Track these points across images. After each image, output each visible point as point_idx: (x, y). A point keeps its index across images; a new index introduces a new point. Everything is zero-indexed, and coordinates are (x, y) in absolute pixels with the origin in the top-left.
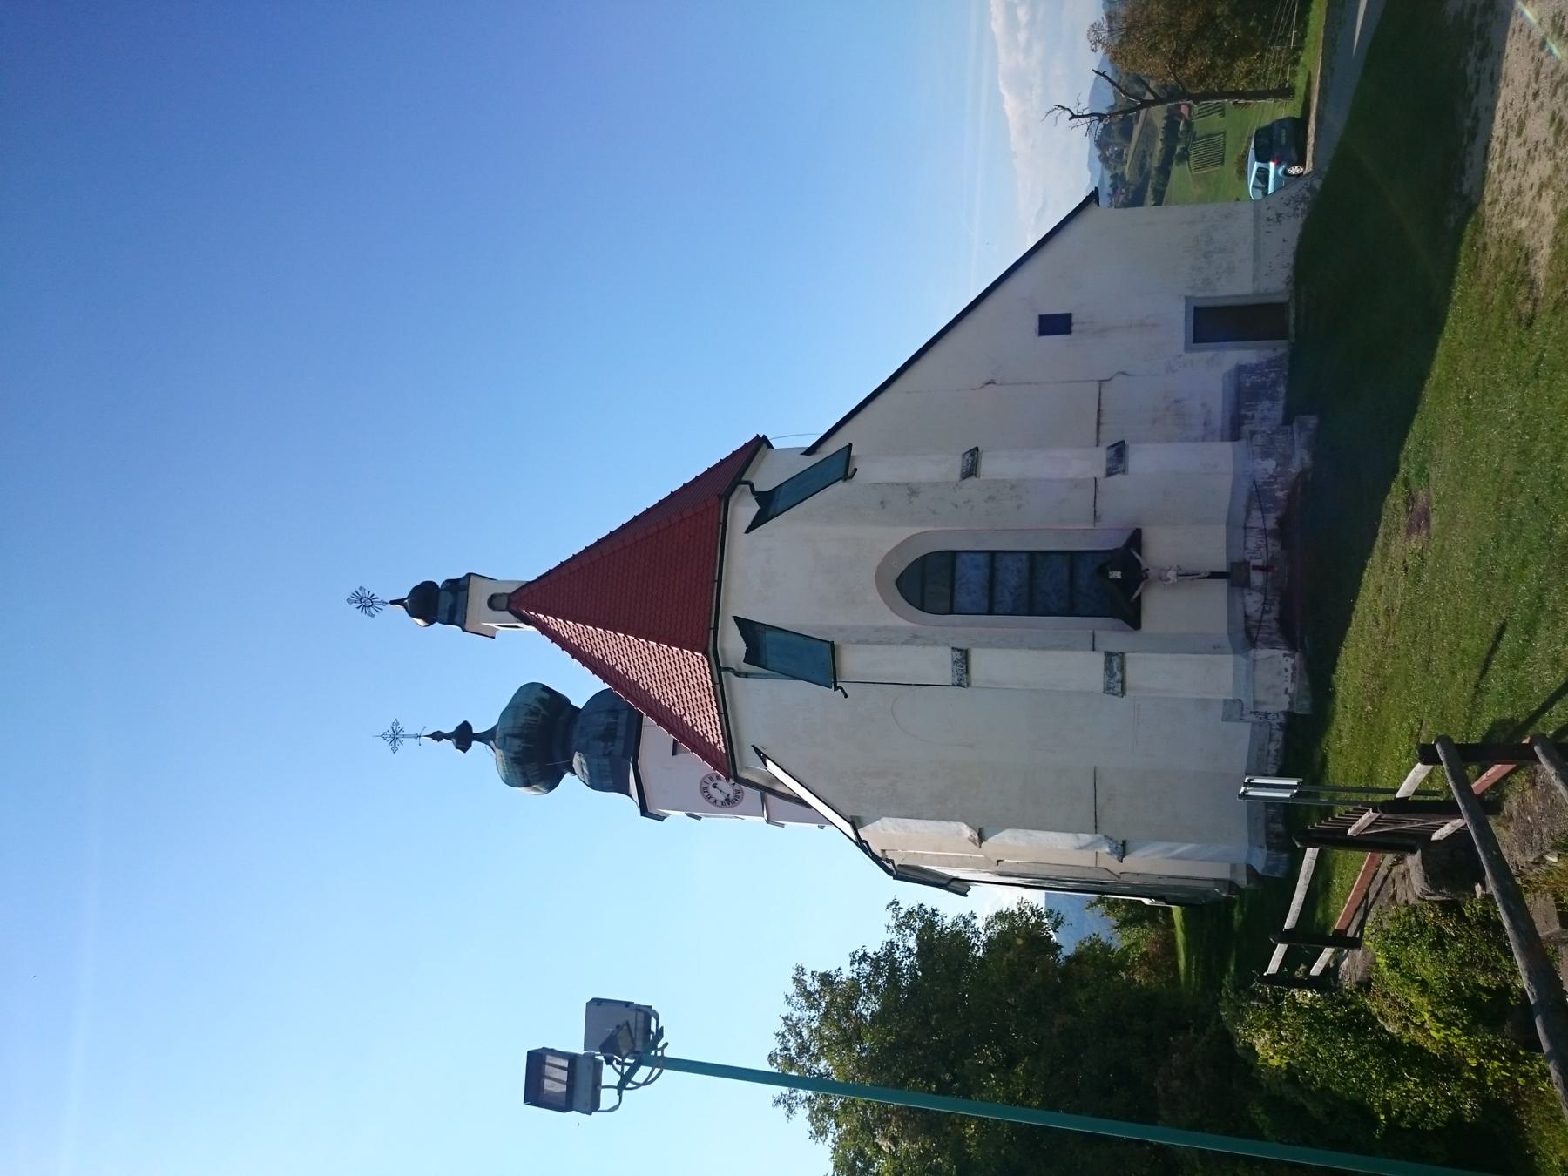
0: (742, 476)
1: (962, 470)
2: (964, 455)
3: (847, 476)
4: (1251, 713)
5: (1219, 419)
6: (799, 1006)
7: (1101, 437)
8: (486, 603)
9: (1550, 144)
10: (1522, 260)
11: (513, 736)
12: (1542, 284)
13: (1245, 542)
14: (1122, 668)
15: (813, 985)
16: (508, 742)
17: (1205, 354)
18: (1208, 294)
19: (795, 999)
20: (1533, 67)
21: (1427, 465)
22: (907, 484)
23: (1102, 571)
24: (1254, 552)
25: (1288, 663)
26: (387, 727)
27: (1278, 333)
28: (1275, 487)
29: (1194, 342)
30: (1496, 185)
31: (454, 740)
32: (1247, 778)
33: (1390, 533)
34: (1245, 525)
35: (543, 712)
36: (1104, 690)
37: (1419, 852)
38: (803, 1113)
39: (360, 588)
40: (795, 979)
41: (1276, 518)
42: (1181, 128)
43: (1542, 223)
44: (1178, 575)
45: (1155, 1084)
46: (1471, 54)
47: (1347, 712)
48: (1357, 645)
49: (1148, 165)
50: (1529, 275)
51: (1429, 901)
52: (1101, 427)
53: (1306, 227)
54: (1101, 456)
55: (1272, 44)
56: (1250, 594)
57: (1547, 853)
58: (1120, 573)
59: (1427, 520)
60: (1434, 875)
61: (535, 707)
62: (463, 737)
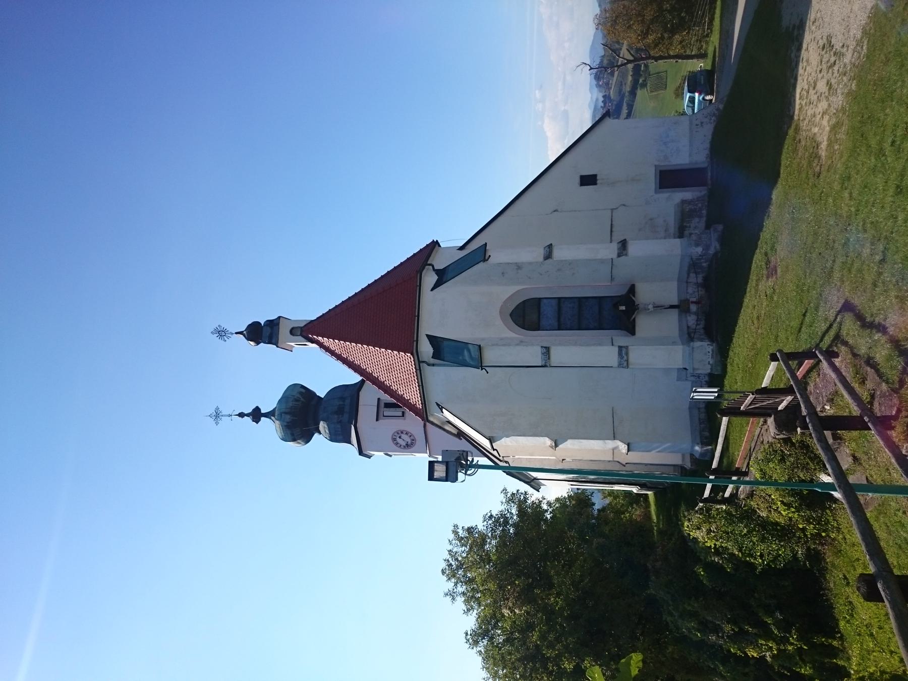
0: (428, 260)
1: (544, 255)
2: (545, 248)
3: (485, 260)
4: (691, 376)
5: (672, 229)
6: (456, 545)
7: (613, 238)
8: (289, 331)
9: (827, 94)
10: (815, 147)
11: (286, 413)
12: (823, 158)
13: (687, 290)
14: (627, 354)
15: (461, 533)
16: (283, 416)
17: (665, 195)
18: (667, 163)
19: (454, 542)
20: (819, 58)
21: (775, 245)
22: (516, 263)
23: (616, 306)
24: (691, 294)
25: (710, 349)
26: (212, 411)
27: (702, 184)
28: (702, 261)
29: (660, 188)
30: (805, 111)
31: (251, 417)
32: (694, 389)
33: (759, 279)
34: (687, 281)
35: (302, 399)
36: (618, 365)
37: (773, 416)
38: (460, 600)
39: (219, 326)
40: (453, 531)
41: (703, 277)
42: (642, 69)
43: (824, 130)
44: (654, 307)
45: (648, 565)
46: (793, 48)
47: (739, 370)
48: (744, 336)
49: (624, 90)
50: (818, 154)
51: (778, 439)
52: (613, 233)
53: (716, 129)
54: (614, 248)
55: (694, 26)
56: (690, 316)
57: (825, 405)
58: (624, 307)
59: (776, 271)
60: (780, 426)
61: (298, 397)
62: (256, 415)
